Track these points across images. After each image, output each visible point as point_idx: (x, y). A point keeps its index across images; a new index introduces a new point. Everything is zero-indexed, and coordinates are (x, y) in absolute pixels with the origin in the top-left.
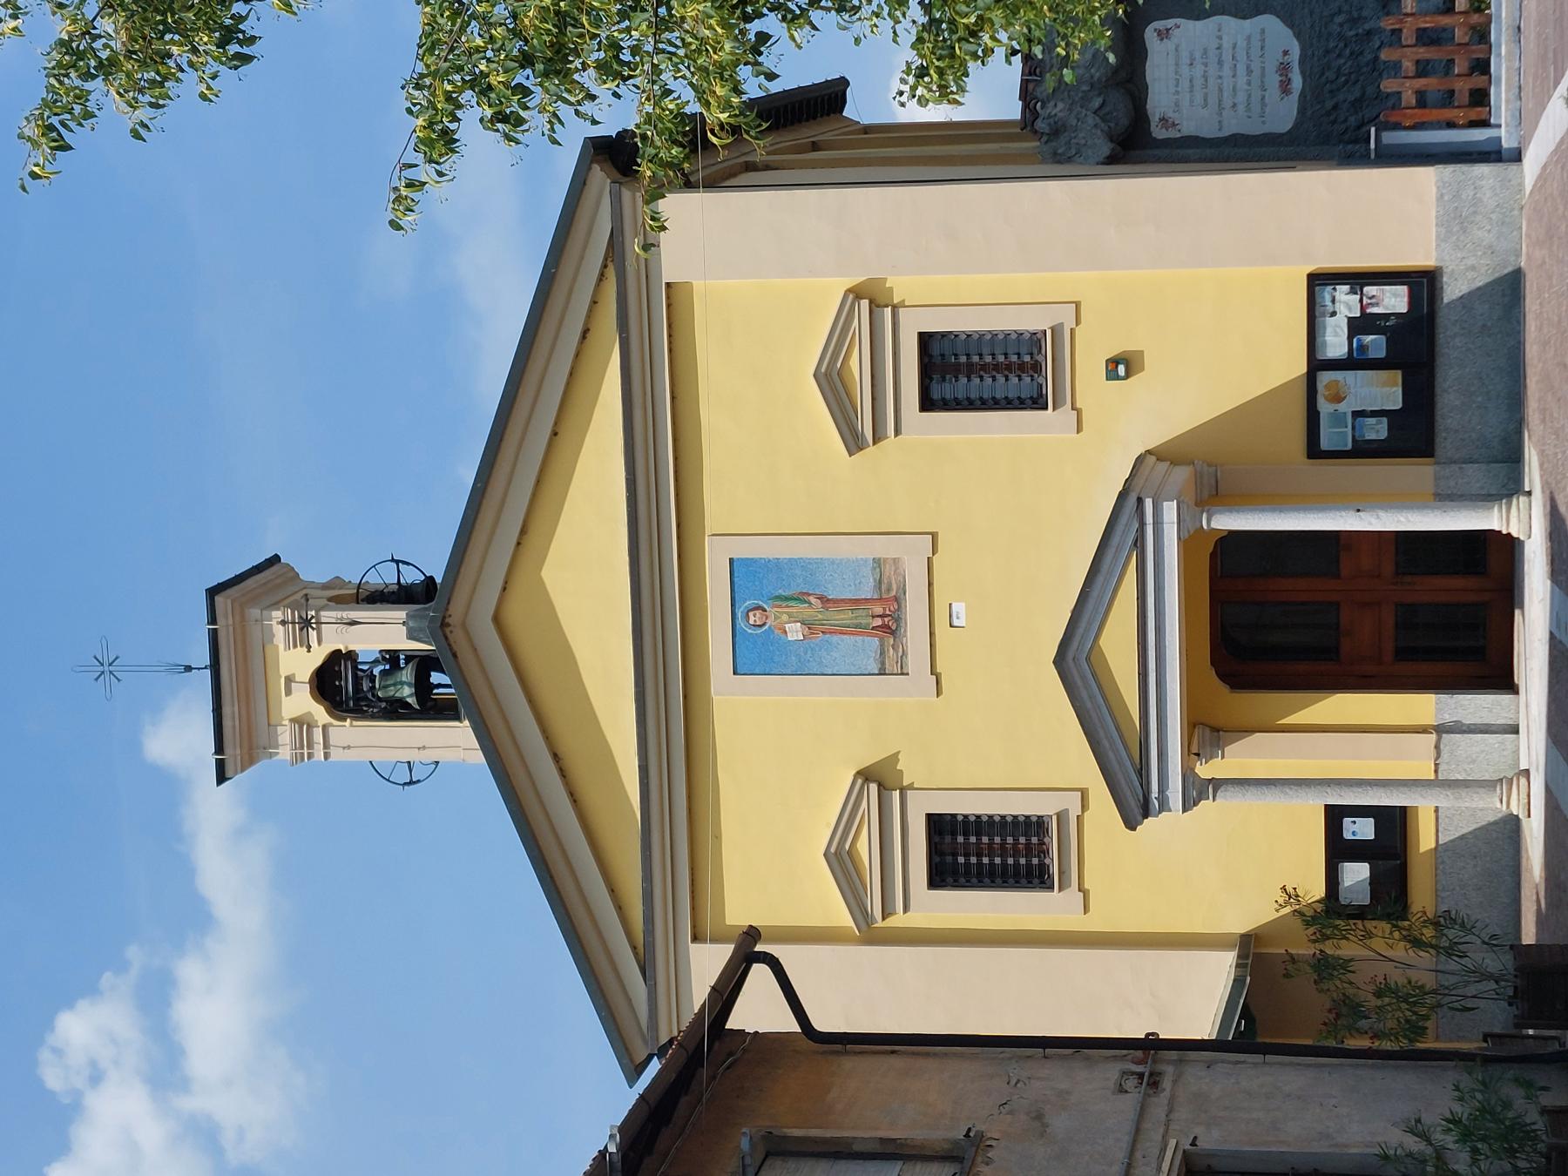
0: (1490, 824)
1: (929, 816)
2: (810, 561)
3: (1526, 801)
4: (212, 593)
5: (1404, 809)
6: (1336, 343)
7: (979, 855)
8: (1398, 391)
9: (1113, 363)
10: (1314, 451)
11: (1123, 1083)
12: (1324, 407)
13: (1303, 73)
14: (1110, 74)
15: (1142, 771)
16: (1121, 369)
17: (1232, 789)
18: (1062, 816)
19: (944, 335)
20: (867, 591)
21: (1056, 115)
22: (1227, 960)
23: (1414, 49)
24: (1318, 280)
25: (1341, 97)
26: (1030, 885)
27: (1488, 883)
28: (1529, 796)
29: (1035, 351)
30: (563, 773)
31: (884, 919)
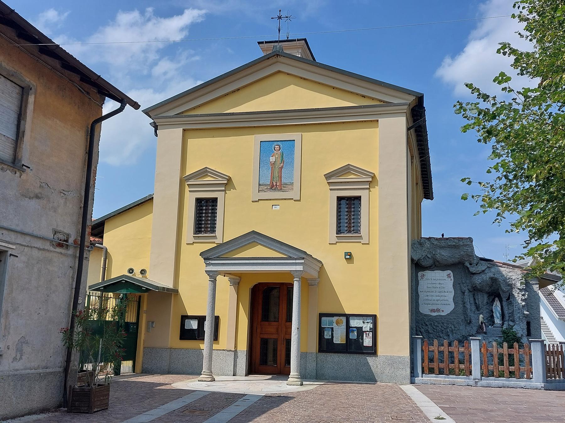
1: (217, 199)
2: (293, 163)
4: (305, 40)
6: (355, 323)
7: (206, 213)
9: (350, 255)
10: (321, 315)
11: (61, 233)
12: (335, 319)
13: (437, 316)
14: (437, 260)
15: (218, 258)
16: (348, 257)
18: (215, 237)
19: (360, 204)
20: (284, 181)
21: (426, 244)
22: (169, 285)
23: (447, 351)
24: (374, 317)
25: (429, 327)
28: (205, 381)
29: (355, 232)
30: (234, 92)
31: (188, 185)
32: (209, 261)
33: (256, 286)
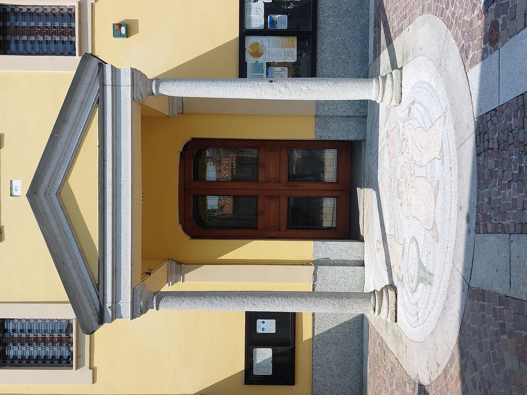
0: (345, 323)
3: (394, 309)
5: (294, 314)
8: (294, 51)
15: (100, 286)
16: (123, 30)
17: (172, 300)
26: (61, 365)
27: (344, 361)
28: (396, 305)
32: (106, 311)
33: (186, 230)
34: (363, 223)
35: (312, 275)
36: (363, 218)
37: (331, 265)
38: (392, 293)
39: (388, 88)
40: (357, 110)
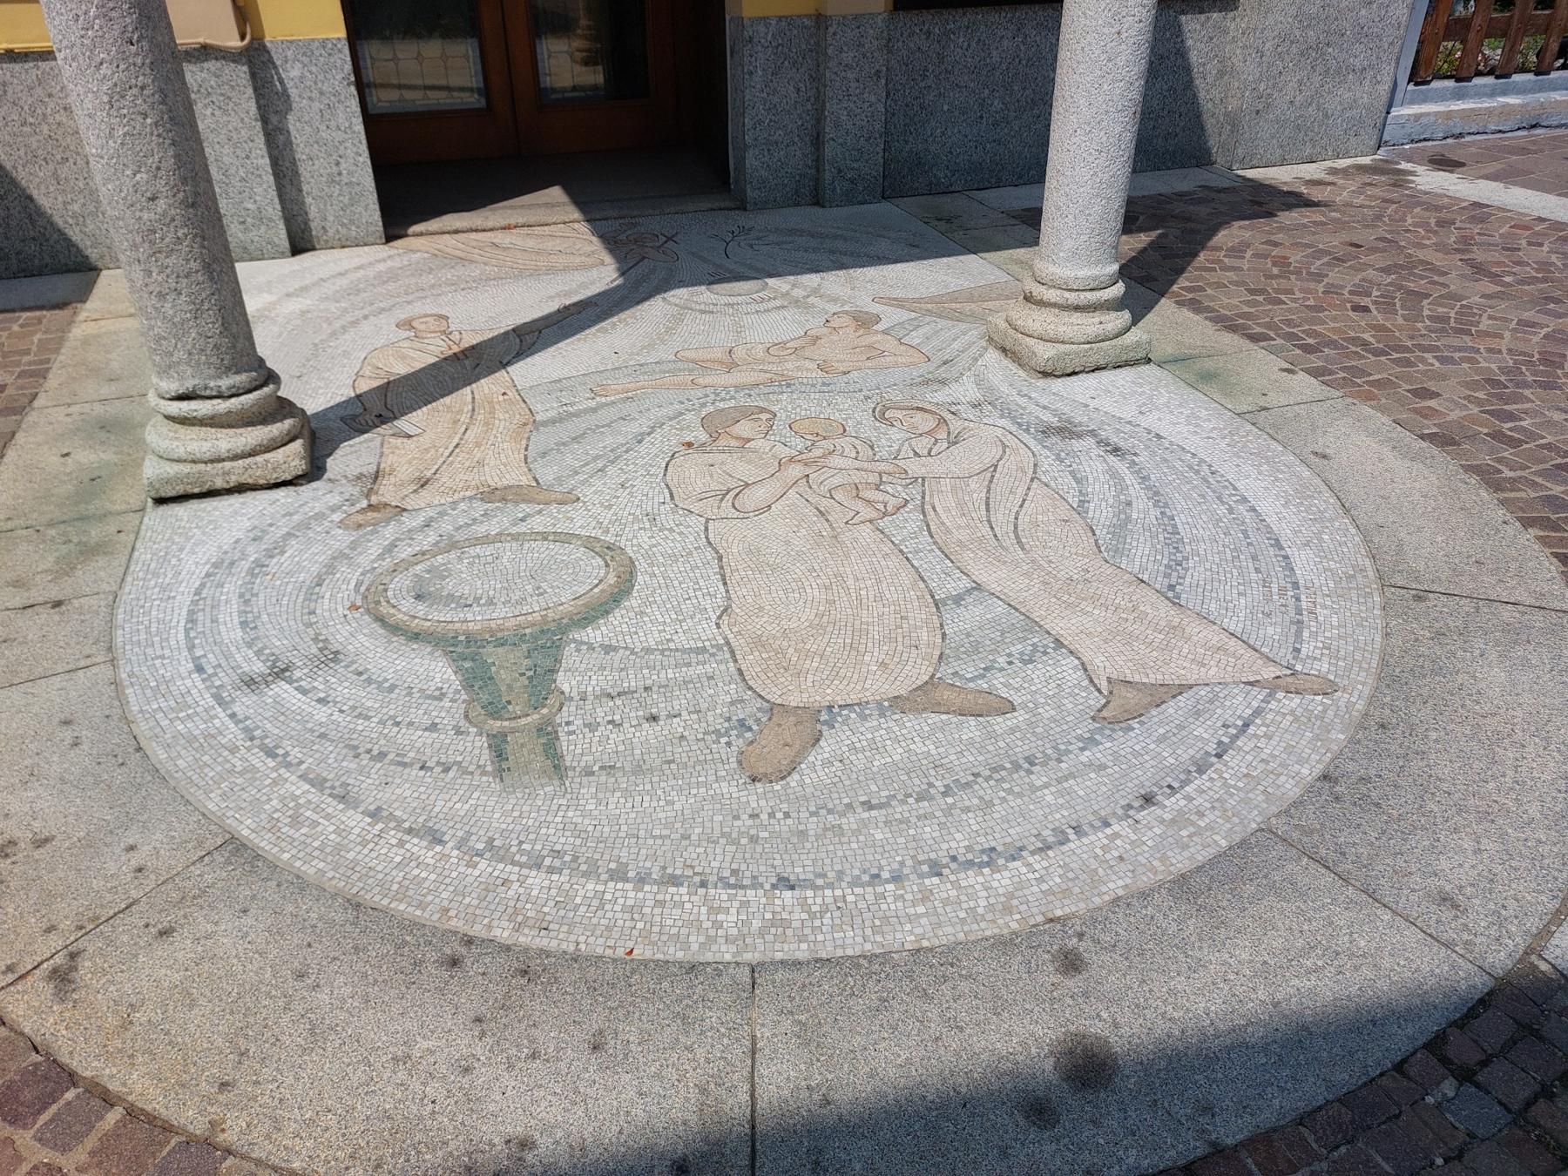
3: (219, 483)
28: (241, 489)
34: (457, 232)
35: (201, 40)
36: (474, 227)
37: (265, 121)
38: (293, 464)
39: (1092, 325)
40: (840, 171)
